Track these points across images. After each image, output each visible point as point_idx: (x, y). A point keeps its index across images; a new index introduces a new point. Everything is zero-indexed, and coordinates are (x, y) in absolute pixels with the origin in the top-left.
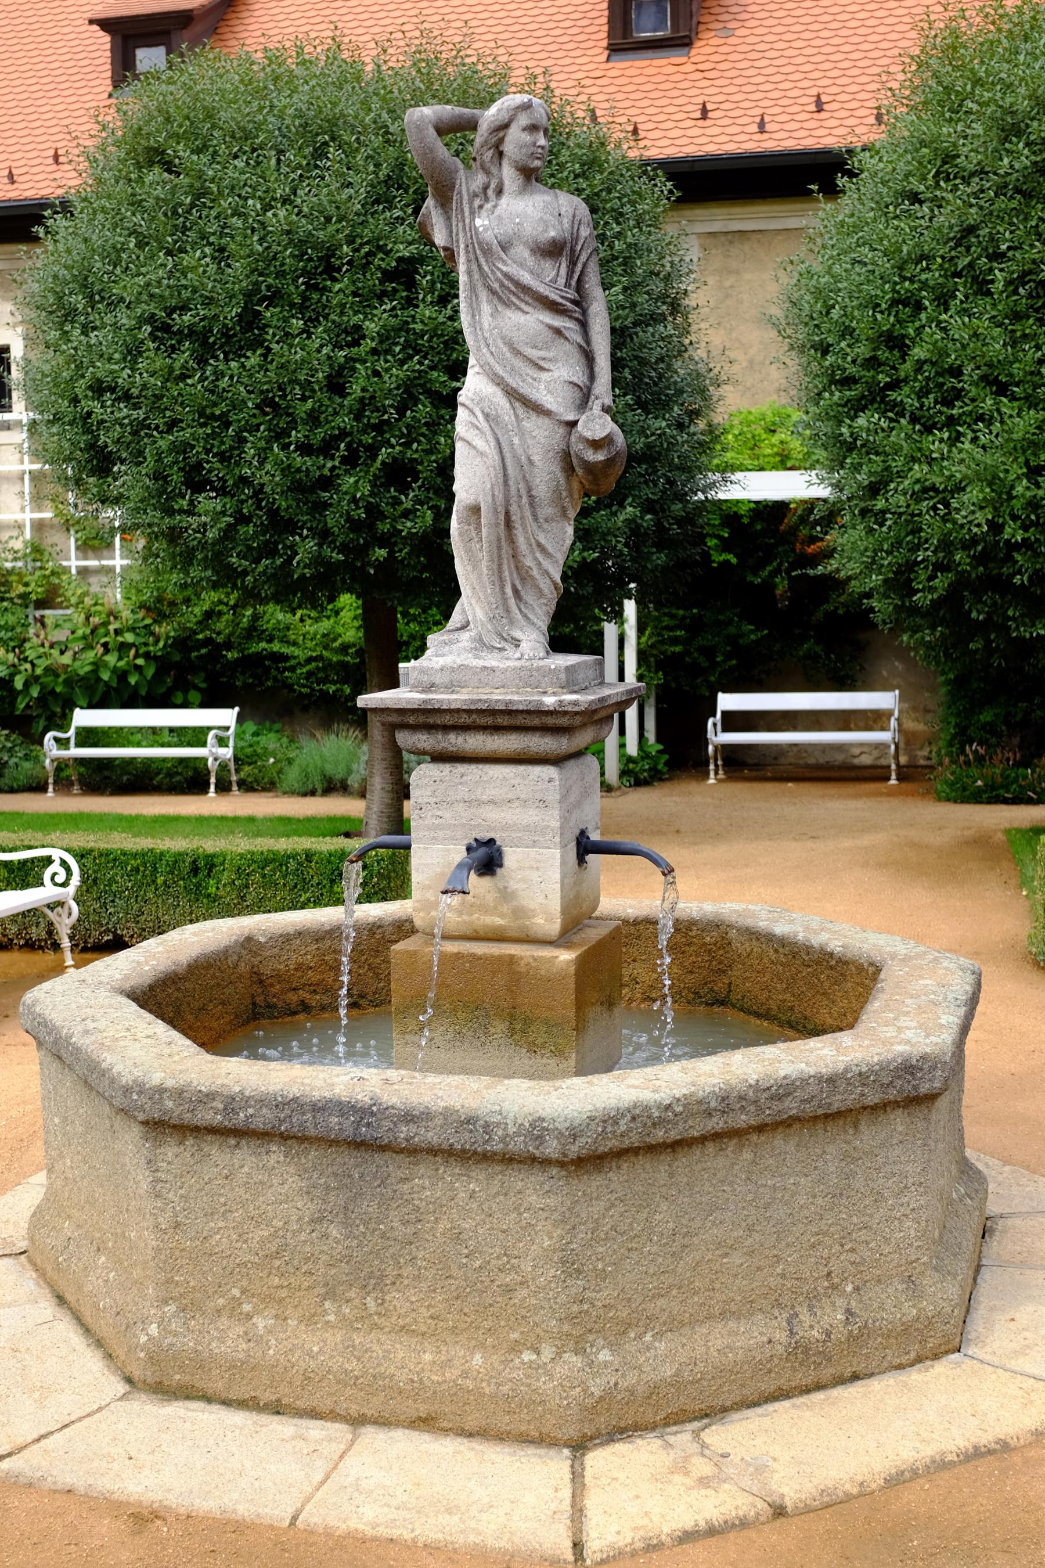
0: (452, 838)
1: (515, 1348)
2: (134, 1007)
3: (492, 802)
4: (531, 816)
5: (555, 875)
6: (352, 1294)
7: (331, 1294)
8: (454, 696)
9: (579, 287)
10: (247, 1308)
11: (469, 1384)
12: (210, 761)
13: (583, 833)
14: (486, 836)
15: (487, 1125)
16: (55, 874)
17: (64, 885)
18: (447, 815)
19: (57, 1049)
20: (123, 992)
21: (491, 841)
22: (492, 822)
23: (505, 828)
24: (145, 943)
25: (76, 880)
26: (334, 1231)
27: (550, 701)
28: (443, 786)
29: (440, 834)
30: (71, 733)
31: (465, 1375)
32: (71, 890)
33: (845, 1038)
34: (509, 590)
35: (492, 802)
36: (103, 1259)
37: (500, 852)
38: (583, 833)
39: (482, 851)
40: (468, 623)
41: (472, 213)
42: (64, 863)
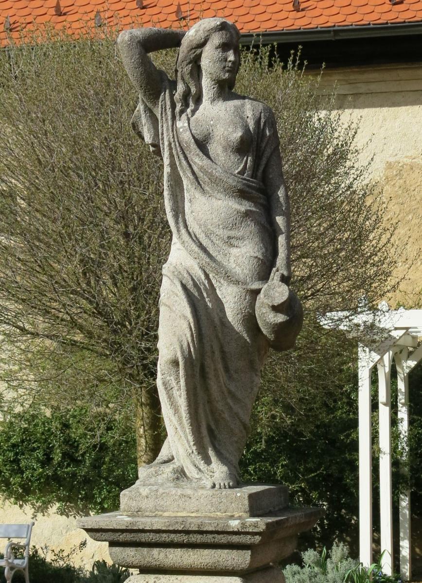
40: (173, 459)
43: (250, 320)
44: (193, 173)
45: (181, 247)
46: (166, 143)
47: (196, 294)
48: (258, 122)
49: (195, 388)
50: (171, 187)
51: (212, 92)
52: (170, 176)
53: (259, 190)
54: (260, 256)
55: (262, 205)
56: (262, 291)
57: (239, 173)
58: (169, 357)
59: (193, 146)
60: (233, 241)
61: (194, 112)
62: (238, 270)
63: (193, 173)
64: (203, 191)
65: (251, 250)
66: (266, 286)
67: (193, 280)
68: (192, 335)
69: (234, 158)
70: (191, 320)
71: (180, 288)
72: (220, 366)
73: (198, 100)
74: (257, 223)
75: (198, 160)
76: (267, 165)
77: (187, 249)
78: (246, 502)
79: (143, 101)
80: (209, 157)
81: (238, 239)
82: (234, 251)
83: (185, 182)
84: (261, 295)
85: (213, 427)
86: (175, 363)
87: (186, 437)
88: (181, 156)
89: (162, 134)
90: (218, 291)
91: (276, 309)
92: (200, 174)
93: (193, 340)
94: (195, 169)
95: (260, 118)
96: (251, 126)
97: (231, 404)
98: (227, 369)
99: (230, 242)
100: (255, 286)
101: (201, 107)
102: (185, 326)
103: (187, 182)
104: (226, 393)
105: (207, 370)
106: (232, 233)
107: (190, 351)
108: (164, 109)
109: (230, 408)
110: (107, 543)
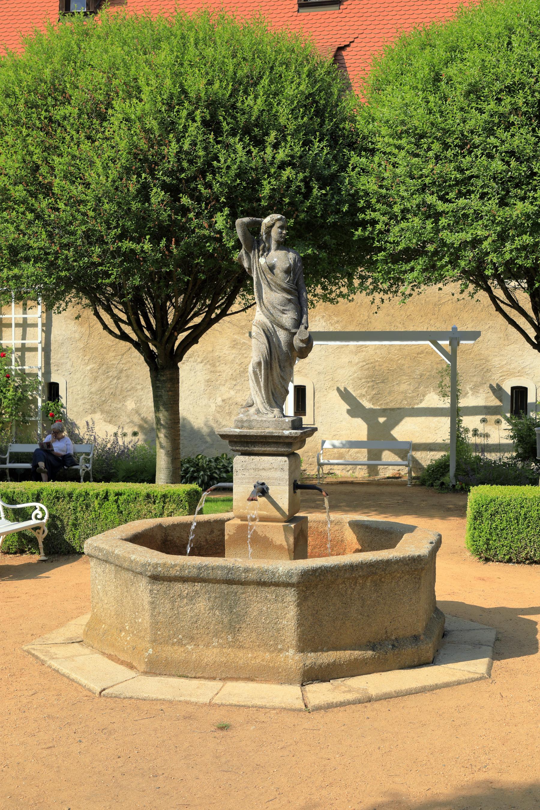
0: (249, 483)
1: (280, 651)
2: (131, 544)
3: (263, 469)
4: (278, 474)
5: (287, 495)
6: (223, 635)
7: (216, 636)
8: (251, 430)
9: (297, 284)
10: (184, 642)
11: (264, 663)
12: (81, 471)
13: (295, 481)
14: (261, 481)
15: (273, 572)
16: (37, 514)
17: (42, 518)
18: (247, 474)
19: (105, 560)
20: (126, 540)
21: (263, 484)
22: (264, 477)
23: (269, 478)
24: (110, 531)
25: (46, 517)
26: (217, 613)
27: (287, 433)
28: (245, 463)
29: (244, 481)
30: (8, 455)
31: (263, 660)
32: (44, 521)
33: (391, 550)
34: (271, 394)
35: (263, 469)
36: (123, 633)
37: (268, 488)
38: (295, 481)
39: (260, 486)
40: (253, 404)
41: (259, 257)
42: (41, 509)
43: (290, 344)
47: (190, 331)
48: (295, 261)
50: (257, 287)
53: (295, 289)
54: (295, 317)
61: (267, 255)
62: (287, 324)
64: (271, 289)
72: (277, 365)
73: (269, 250)
78: (290, 424)
82: (285, 316)
84: (297, 335)
86: (259, 364)
91: (302, 341)
94: (269, 280)
98: (280, 366)
100: (293, 331)
103: (264, 286)
106: (284, 308)
108: (254, 254)
109: (281, 383)
110: (228, 441)
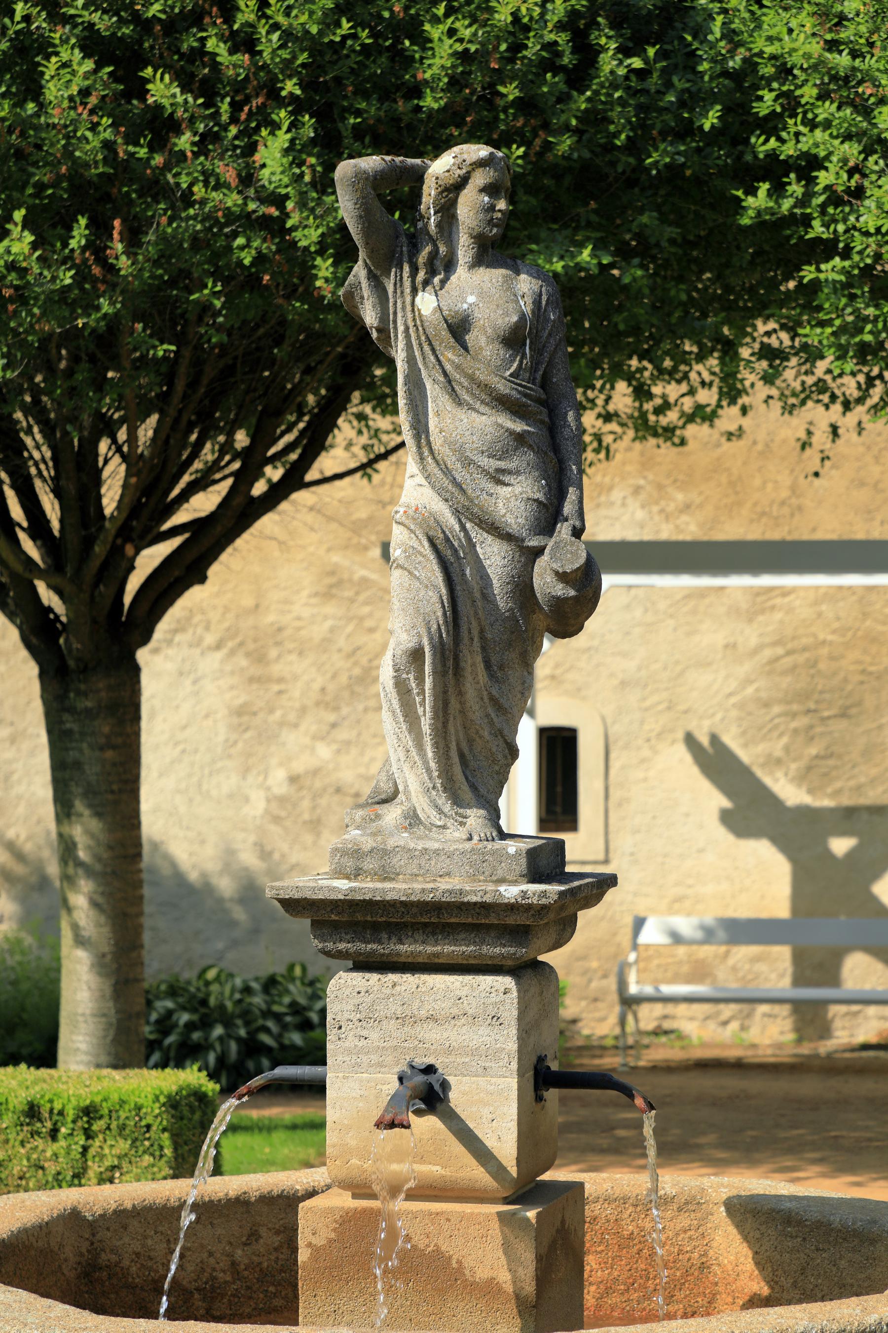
44: (445, 374)
45: (423, 482)
46: (401, 328)
48: (537, 302)
49: (445, 692)
50: (409, 392)
51: (471, 253)
52: (407, 377)
53: (539, 401)
54: (540, 496)
55: (542, 422)
56: (547, 551)
57: (511, 375)
58: (410, 645)
59: (445, 333)
60: (506, 478)
61: (443, 282)
62: (510, 519)
63: (445, 374)
64: (458, 401)
65: (529, 490)
66: (551, 543)
67: (444, 532)
68: (445, 614)
69: (504, 353)
70: (444, 591)
71: (426, 544)
72: (479, 659)
73: (450, 265)
74: (538, 452)
75: (450, 356)
76: (550, 364)
77: (433, 487)
78: (523, 861)
79: (366, 265)
80: (466, 349)
81: (510, 472)
83: (429, 385)
85: (466, 751)
86: (416, 655)
87: (426, 763)
88: (426, 348)
89: (395, 313)
90: (478, 549)
91: (562, 577)
92: (456, 375)
93: (446, 622)
94: (448, 367)
95: (540, 295)
96: (528, 309)
97: (493, 715)
99: (498, 478)
101: (453, 278)
102: (435, 599)
103: (433, 390)
104: (486, 700)
105: (462, 664)
106: (502, 464)
107: (441, 636)
110: (308, 922)
